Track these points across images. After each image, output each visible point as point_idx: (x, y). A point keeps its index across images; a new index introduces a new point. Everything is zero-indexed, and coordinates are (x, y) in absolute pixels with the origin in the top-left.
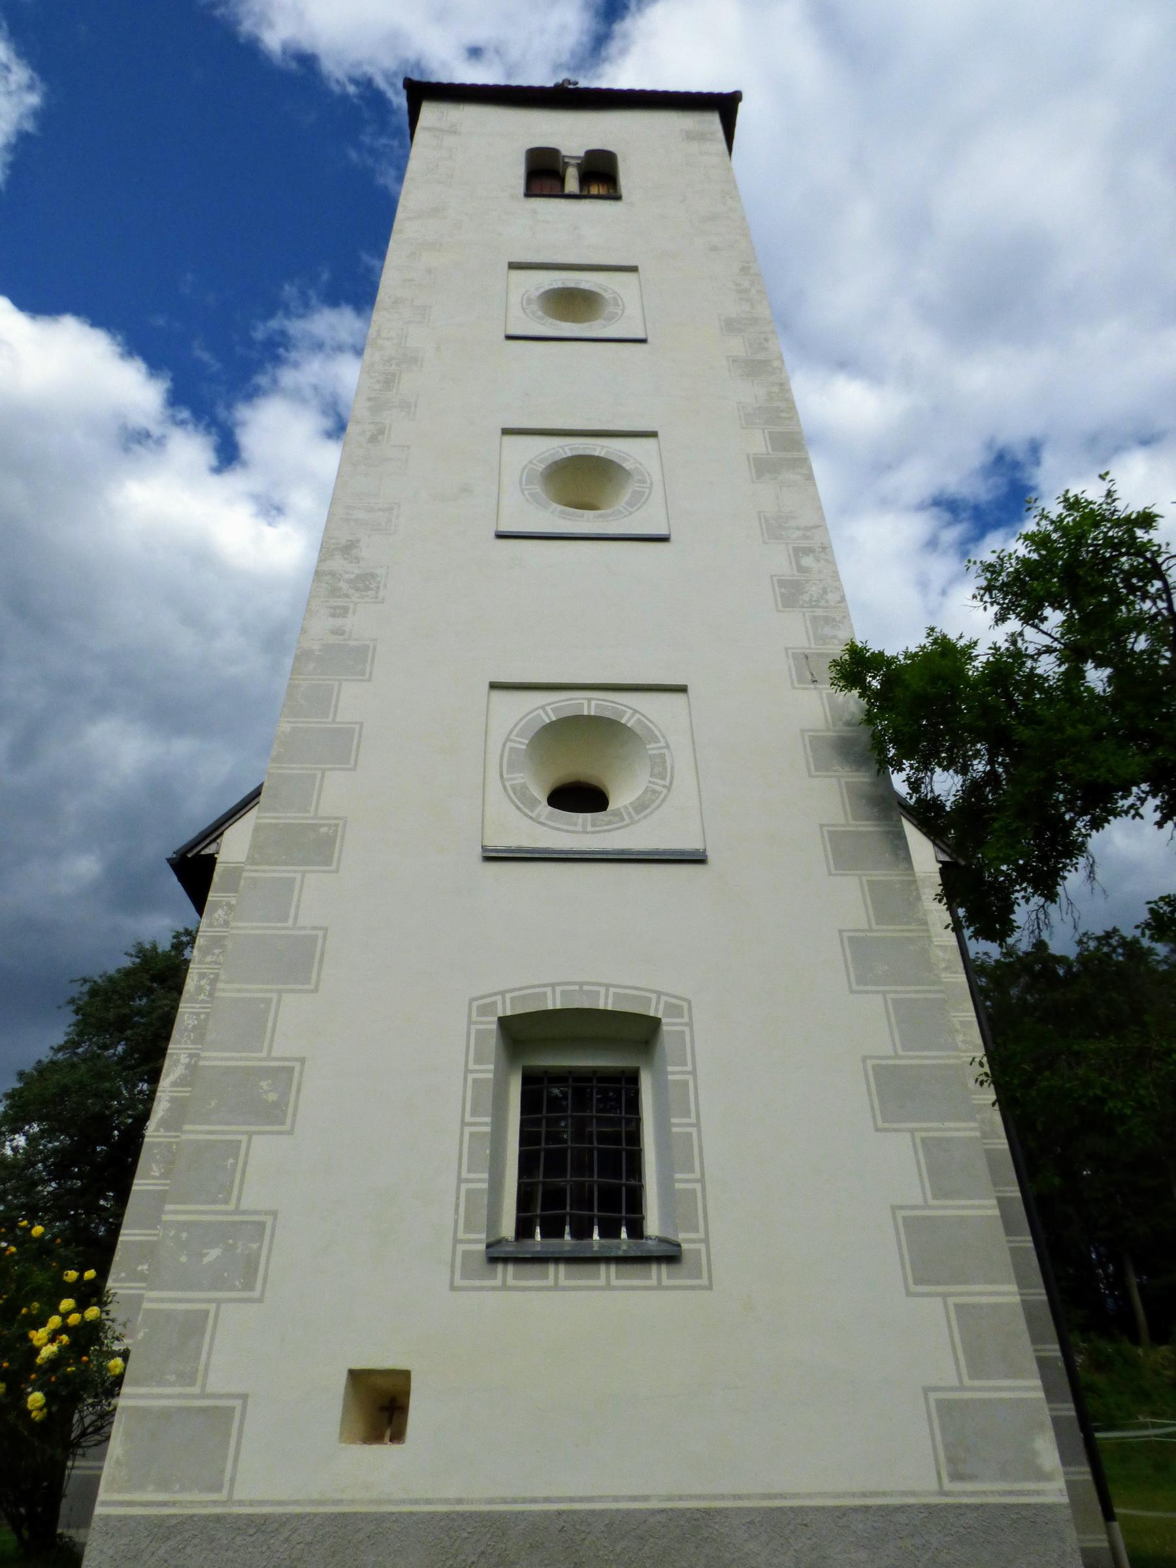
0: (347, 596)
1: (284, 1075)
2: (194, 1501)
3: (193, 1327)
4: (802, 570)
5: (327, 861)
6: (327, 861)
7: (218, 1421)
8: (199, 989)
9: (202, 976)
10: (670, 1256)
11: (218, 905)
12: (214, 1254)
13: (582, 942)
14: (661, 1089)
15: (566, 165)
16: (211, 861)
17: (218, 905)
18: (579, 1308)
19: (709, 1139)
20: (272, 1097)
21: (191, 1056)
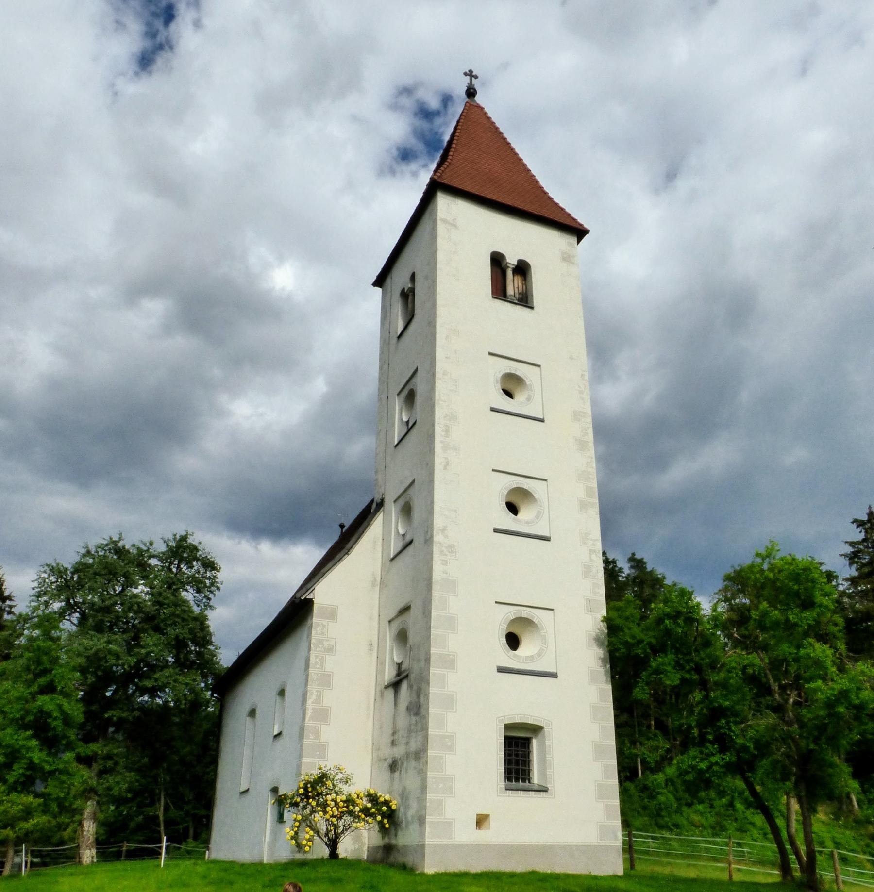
0: (446, 555)
1: (451, 737)
2: (446, 841)
3: (440, 802)
4: (591, 560)
5: (453, 668)
6: (453, 668)
7: (448, 825)
8: (316, 663)
9: (316, 657)
10: (544, 790)
11: (318, 625)
12: (441, 786)
13: (523, 702)
14: (542, 746)
15: (508, 267)
16: (309, 603)
17: (318, 625)
18: (521, 801)
19: (550, 758)
20: (449, 744)
21: (317, 691)
